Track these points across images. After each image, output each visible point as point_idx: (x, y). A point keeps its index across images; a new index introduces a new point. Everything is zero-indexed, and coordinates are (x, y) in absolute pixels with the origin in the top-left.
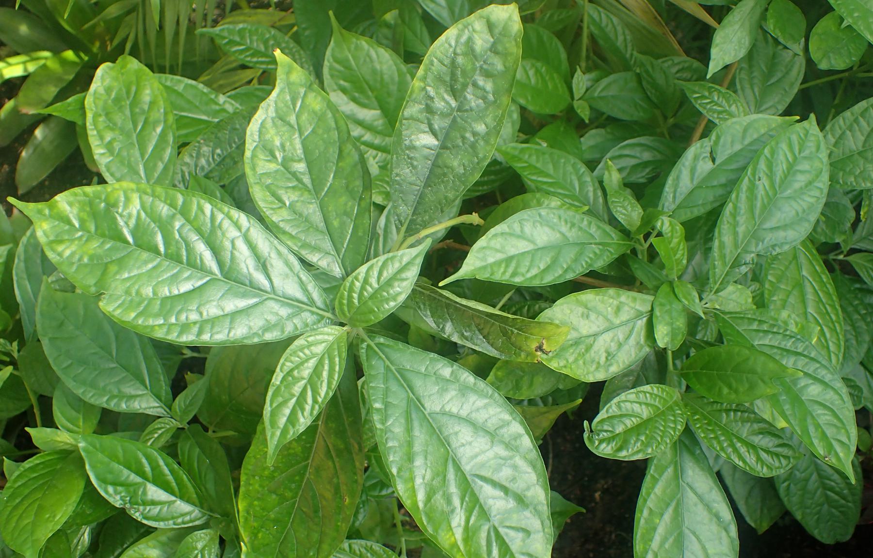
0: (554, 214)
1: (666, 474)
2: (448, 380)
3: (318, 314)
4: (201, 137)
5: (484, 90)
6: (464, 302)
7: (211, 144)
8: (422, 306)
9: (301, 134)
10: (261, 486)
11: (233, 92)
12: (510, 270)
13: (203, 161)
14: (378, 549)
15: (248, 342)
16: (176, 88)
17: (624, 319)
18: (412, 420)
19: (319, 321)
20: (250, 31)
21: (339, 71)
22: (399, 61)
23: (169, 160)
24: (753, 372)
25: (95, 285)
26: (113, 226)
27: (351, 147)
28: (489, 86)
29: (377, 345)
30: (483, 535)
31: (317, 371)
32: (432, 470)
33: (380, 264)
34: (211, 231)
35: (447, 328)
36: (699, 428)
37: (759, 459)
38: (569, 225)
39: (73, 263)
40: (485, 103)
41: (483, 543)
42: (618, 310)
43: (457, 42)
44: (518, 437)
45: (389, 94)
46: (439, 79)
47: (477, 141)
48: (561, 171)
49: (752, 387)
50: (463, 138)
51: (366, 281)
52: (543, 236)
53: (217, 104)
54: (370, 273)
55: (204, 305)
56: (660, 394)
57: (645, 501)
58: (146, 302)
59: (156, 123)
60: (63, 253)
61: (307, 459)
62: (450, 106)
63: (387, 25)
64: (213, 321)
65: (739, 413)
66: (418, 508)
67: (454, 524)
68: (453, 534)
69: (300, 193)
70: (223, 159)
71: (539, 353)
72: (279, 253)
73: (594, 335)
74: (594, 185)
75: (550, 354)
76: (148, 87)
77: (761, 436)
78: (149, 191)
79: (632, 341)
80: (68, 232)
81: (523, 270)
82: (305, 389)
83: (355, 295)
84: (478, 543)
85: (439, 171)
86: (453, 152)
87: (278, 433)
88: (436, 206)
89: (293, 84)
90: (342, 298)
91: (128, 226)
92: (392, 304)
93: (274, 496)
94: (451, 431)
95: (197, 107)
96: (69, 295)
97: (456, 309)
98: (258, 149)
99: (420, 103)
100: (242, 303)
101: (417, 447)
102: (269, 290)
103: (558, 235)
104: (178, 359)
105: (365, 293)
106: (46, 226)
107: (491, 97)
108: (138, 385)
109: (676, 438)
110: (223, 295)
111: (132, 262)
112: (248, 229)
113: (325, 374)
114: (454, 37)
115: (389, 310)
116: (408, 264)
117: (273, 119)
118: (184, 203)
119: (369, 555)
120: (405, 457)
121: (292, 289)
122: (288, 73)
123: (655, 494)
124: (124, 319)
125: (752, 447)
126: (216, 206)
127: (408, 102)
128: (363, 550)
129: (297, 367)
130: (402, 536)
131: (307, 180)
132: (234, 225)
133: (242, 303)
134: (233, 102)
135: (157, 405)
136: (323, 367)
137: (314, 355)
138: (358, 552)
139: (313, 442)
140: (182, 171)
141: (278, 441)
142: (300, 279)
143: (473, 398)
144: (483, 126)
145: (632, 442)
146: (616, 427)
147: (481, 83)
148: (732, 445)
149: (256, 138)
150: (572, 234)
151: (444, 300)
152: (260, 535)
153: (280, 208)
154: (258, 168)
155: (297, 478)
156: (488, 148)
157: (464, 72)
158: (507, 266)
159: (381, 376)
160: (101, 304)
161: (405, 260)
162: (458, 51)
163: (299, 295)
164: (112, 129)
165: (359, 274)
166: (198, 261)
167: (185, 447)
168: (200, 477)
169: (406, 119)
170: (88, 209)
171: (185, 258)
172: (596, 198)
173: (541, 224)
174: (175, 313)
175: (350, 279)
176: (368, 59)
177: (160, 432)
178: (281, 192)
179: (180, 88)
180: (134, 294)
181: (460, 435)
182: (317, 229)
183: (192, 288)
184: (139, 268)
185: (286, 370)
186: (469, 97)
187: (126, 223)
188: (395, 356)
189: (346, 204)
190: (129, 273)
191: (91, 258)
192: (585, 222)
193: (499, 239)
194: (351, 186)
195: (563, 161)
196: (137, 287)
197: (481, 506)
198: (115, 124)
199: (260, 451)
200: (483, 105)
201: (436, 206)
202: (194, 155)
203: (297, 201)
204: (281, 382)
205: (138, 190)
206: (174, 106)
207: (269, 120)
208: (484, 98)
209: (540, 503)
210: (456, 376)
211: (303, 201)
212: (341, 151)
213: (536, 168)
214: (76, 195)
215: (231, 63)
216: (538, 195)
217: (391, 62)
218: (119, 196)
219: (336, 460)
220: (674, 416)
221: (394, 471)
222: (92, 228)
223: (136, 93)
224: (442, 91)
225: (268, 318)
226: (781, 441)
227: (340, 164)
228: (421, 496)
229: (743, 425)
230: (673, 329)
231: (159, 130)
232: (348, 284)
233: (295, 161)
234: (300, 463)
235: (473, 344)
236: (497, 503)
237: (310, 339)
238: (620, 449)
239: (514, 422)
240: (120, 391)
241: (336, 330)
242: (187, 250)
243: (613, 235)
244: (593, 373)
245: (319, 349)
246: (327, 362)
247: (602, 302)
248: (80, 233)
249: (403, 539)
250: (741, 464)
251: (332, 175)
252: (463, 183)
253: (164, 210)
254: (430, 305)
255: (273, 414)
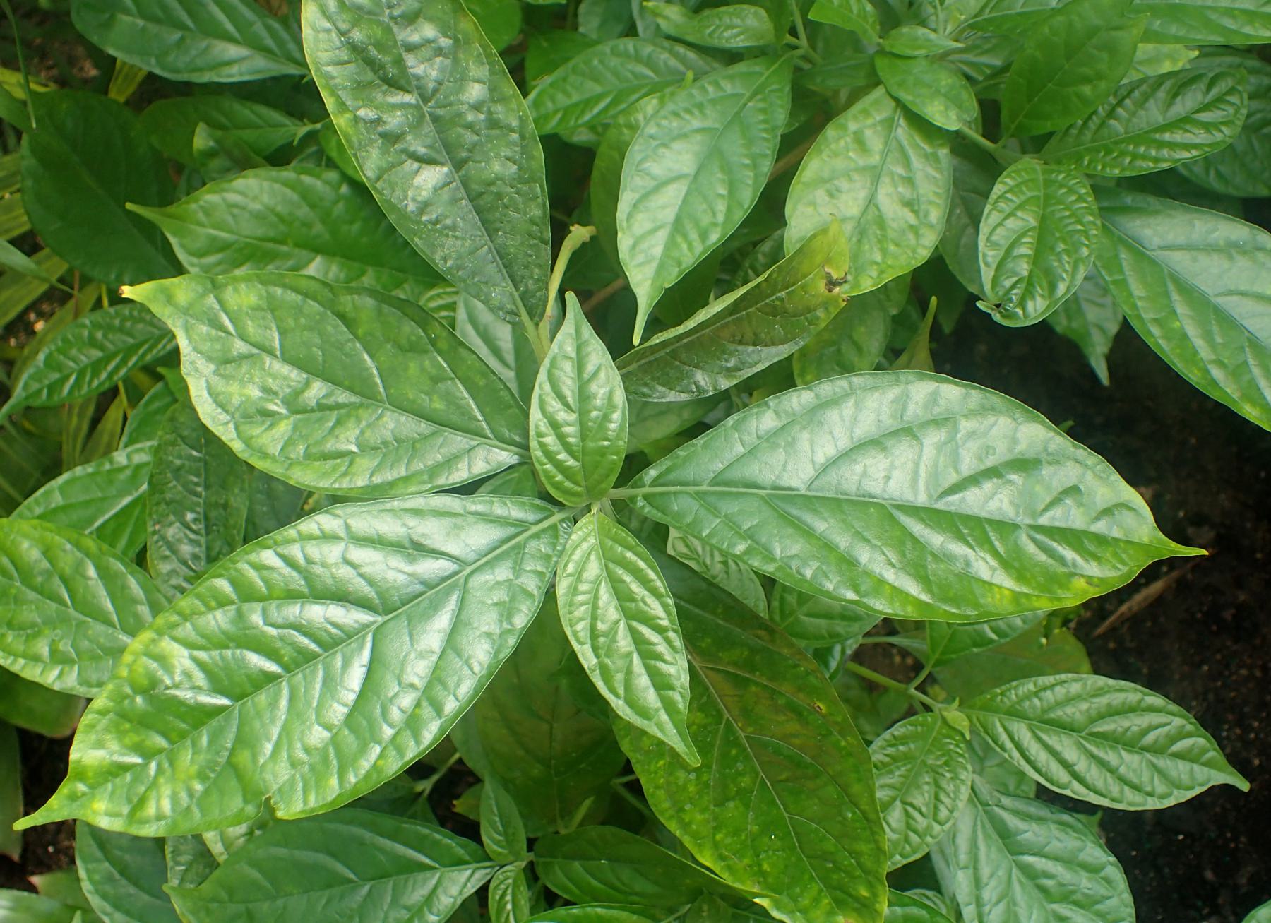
0: (665, 118)
1: (1124, 264)
2: (783, 428)
3: (544, 531)
4: (150, 523)
5: (429, 41)
6: (691, 324)
7: (172, 518)
8: (645, 390)
9: (271, 353)
10: (702, 811)
11: (124, 439)
12: (694, 236)
13: (186, 549)
14: (903, 730)
15: (506, 653)
16: (53, 505)
17: (881, 147)
18: (798, 519)
19: (556, 536)
20: (58, 350)
21: (219, 263)
22: (273, 172)
23: (146, 591)
24: (1093, 32)
25: (246, 801)
26: (183, 709)
27: (349, 298)
28: (429, 31)
29: (652, 485)
30: (1031, 548)
31: (623, 596)
32: (890, 545)
33: (547, 387)
34: (306, 579)
35: (702, 383)
36: (1103, 168)
37: (1207, 126)
38: (696, 112)
39: (188, 808)
40: (445, 56)
41: (1043, 557)
42: (860, 141)
43: (328, 17)
44: (934, 399)
45: (308, 225)
46: (360, 88)
47: (490, 113)
48: (609, 75)
49: (1111, 48)
50: (470, 126)
51: (555, 425)
52: (680, 159)
53: (121, 469)
54: (549, 416)
55: (402, 671)
56: (1019, 180)
57: (1139, 317)
58: (331, 750)
59: (79, 568)
60: (161, 811)
61: (719, 715)
62: (409, 105)
63: (210, 154)
64: (437, 677)
65: (1127, 101)
66: (927, 604)
67: (985, 574)
68: (1000, 587)
69: (353, 420)
70: (206, 518)
71: (837, 290)
72: (417, 512)
73: (868, 202)
74: (663, 48)
75: (849, 278)
76: (19, 539)
77: (1179, 99)
78: (175, 618)
79: (917, 162)
80: (136, 780)
81: (706, 220)
82: (633, 632)
83: (562, 456)
84: (1037, 564)
85: (487, 199)
86: (478, 158)
87: (664, 717)
88: (531, 246)
89: (191, 305)
90: (550, 477)
91: (199, 688)
92: (616, 416)
93: (731, 804)
94: (856, 478)
95: (103, 499)
96: (217, 873)
97: (688, 347)
98: (242, 428)
99: (371, 142)
100: (443, 621)
101: (842, 541)
102: (455, 567)
103: (699, 137)
104: (422, 805)
105: (571, 440)
106: (100, 805)
107: (445, 42)
108: (420, 876)
109: (1095, 207)
110: (411, 636)
111: (257, 724)
112: (347, 526)
113: (636, 588)
114: (319, 15)
115: (621, 426)
116: (579, 350)
117: (216, 373)
118: (233, 583)
119: (901, 748)
120: (844, 567)
121: (479, 537)
122: (170, 299)
123: (1140, 298)
124: (329, 799)
125: (1183, 122)
126: (276, 543)
127: (355, 155)
128: (890, 750)
129: (594, 618)
130: (907, 690)
131: (343, 397)
132: (322, 543)
133: (443, 621)
134: (138, 446)
135: (468, 873)
136: (624, 582)
137: (596, 583)
138: (887, 759)
139: (708, 689)
140: (175, 587)
141: (676, 726)
142: (476, 513)
143: (833, 415)
144: (477, 86)
145: (1055, 264)
146: (1018, 269)
147: (415, 38)
148: (1161, 145)
149: (224, 417)
150: (712, 119)
151: (662, 353)
152: (766, 867)
153: (351, 463)
154: (270, 446)
155: (734, 752)
156: (514, 105)
157: (379, 46)
158: (685, 236)
159: (703, 512)
160: (280, 814)
161: (570, 349)
162: (344, 26)
163: (496, 533)
164: (37, 635)
165: (537, 427)
166: (334, 631)
167: (556, 879)
168: (617, 890)
169: (378, 179)
170: (127, 726)
171: (313, 646)
172: (683, 60)
173: (665, 145)
174: (381, 721)
175: (533, 444)
176: (236, 211)
177: (508, 898)
178: (330, 446)
179: (58, 500)
180: (305, 757)
181: (870, 471)
182: (425, 438)
183: (364, 670)
184: (273, 721)
185: (584, 635)
186: (419, 70)
187: (193, 688)
188: (689, 472)
189: (423, 369)
190: (269, 740)
191: (202, 777)
192: (710, 89)
193: (640, 217)
194: (404, 342)
195: (596, 62)
196: (299, 745)
197: (990, 522)
198: (33, 625)
199: (656, 773)
200: (448, 62)
201: (531, 246)
202: (167, 553)
203: (362, 432)
204: (597, 656)
205: (160, 633)
206: (79, 526)
207: (215, 380)
208: (439, 52)
209: (1047, 441)
210: (787, 413)
211: (369, 426)
212: (342, 317)
213: (576, 105)
214: (92, 727)
215: (78, 429)
216: (621, 120)
217: (266, 184)
218: (146, 668)
219: (756, 677)
220: (1062, 186)
221: (851, 595)
222: (161, 742)
223: (13, 562)
224: (380, 97)
225: (495, 599)
226: (1206, 81)
227: (360, 332)
228: (913, 588)
229: (1146, 110)
230: (945, 95)
231: (91, 572)
232: (539, 454)
233: (302, 391)
234: (717, 730)
235: (752, 366)
236: (992, 500)
237: (571, 568)
238: (1052, 287)
239: (910, 387)
240: (407, 908)
241: (588, 524)
242: (305, 634)
243: (757, 69)
244: (918, 244)
245: (594, 568)
246: (620, 571)
247: (836, 155)
248: (153, 765)
249: (913, 691)
250: (1195, 153)
251: (366, 357)
252: (532, 180)
253: (219, 620)
254: (653, 379)
255: (631, 703)
